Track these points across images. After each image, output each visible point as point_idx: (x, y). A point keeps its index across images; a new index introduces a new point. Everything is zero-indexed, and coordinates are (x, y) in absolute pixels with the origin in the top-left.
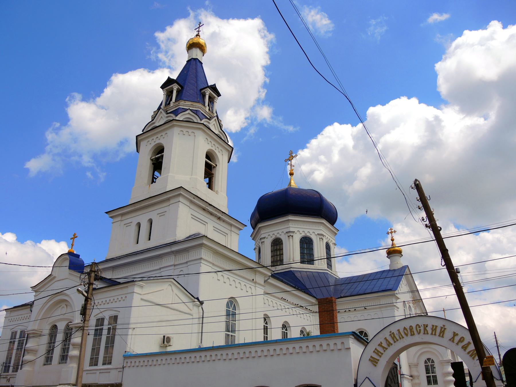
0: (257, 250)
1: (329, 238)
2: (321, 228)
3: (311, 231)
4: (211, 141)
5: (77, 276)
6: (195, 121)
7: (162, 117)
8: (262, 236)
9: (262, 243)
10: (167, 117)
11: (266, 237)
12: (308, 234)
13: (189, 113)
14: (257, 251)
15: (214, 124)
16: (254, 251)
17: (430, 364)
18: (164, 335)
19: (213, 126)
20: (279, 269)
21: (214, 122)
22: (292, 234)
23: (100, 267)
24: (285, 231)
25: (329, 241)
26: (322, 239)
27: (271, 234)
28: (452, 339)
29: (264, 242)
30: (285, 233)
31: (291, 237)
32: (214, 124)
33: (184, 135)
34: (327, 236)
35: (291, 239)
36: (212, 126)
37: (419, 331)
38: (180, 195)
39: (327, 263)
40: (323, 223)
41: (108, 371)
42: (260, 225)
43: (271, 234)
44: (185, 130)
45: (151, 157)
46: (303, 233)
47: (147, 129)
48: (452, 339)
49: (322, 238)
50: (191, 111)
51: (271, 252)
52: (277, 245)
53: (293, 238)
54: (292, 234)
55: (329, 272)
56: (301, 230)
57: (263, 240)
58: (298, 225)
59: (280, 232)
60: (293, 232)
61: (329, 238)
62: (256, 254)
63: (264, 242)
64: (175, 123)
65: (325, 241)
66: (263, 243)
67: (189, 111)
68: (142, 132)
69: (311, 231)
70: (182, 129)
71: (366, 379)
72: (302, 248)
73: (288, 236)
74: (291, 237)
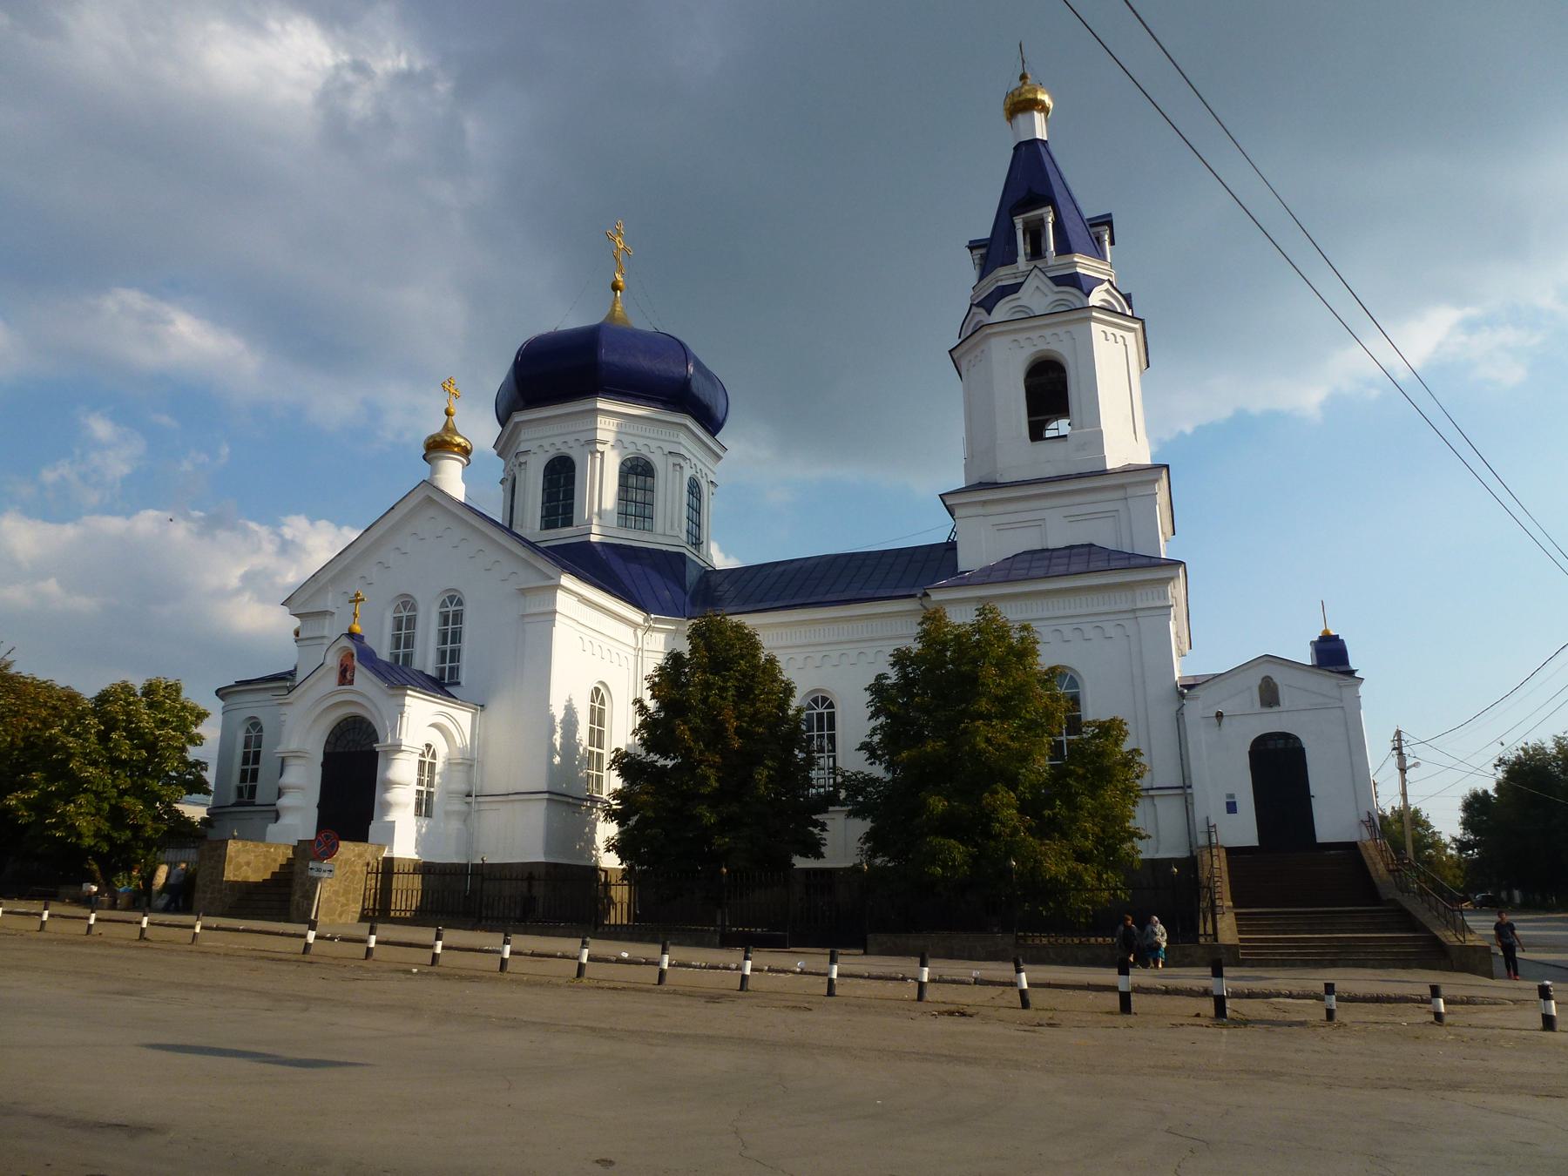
0: (508, 484)
1: (699, 465)
2: (683, 438)
3: (570, 439)
5: (507, 549)
7: (1037, 287)
8: (523, 448)
9: (520, 465)
10: (1057, 293)
12: (645, 451)
14: (508, 486)
15: (1037, 287)
16: (501, 486)
17: (428, 759)
20: (563, 535)
22: (683, 463)
23: (952, 538)
24: (668, 448)
25: (699, 475)
26: (681, 467)
27: (546, 443)
28: (173, 905)
29: (525, 463)
30: (666, 452)
34: (694, 461)
39: (688, 531)
40: (686, 426)
41: (1039, 523)
42: (518, 417)
43: (546, 443)
44: (1019, 336)
47: (965, 334)
48: (173, 905)
49: (679, 465)
55: (689, 552)
57: (522, 459)
58: (640, 429)
59: (570, 439)
60: (685, 458)
61: (699, 465)
62: (505, 496)
63: (525, 463)
64: (989, 331)
65: (688, 473)
66: (523, 467)
68: (960, 340)
69: (653, 445)
72: (623, 485)
73: (674, 465)
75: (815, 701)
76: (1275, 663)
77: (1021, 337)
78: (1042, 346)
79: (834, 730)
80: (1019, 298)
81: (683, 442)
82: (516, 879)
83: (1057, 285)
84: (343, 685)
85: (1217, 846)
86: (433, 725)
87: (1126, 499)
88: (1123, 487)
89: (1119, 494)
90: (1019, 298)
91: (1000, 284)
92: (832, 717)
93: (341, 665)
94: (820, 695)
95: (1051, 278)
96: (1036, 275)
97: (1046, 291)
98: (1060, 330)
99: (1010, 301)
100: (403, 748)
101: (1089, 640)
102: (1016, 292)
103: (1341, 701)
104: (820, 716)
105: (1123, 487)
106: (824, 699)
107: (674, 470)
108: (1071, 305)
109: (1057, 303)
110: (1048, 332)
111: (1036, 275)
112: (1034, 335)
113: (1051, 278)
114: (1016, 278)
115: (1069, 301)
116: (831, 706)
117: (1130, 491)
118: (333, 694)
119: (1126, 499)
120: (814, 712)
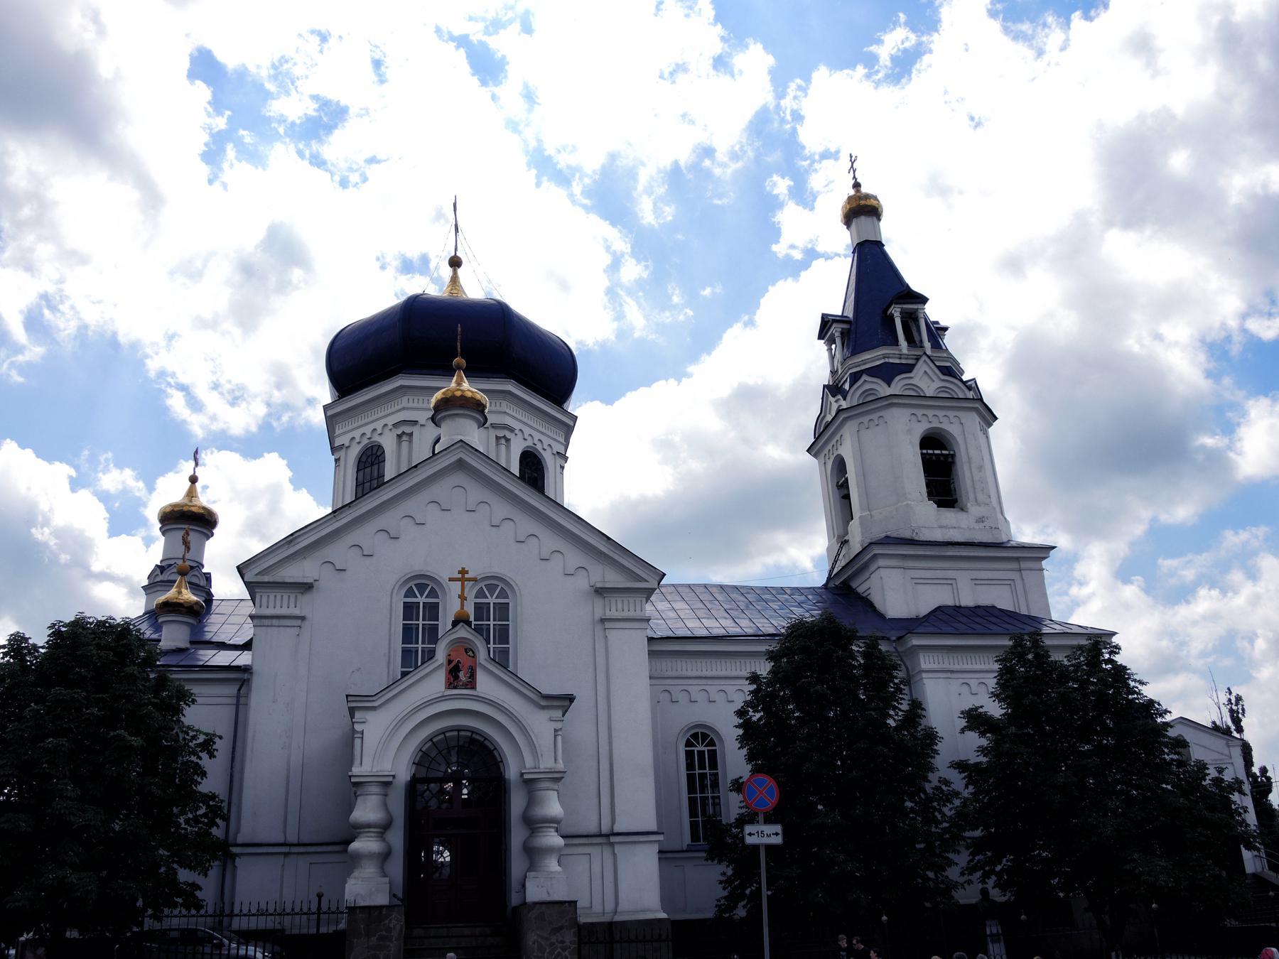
4: (926, 413)
6: (961, 396)
11: (347, 444)
12: (539, 447)
13: (865, 381)
15: (925, 372)
18: (221, 746)
19: (926, 378)
21: (925, 368)
22: (509, 435)
26: (508, 440)
31: (405, 438)
32: (925, 372)
33: (919, 421)
35: (405, 445)
36: (920, 379)
37: (292, 573)
38: (875, 556)
40: (510, 393)
43: (357, 434)
45: (838, 483)
46: (529, 438)
49: (504, 437)
50: (949, 372)
51: (357, 486)
52: (372, 465)
53: (410, 442)
54: (509, 435)
56: (527, 431)
60: (512, 430)
67: (865, 377)
69: (546, 441)
70: (914, 411)
71: (596, 847)
74: (503, 441)
75: (695, 736)
76: (1190, 726)
77: (919, 412)
78: (935, 424)
79: (686, 751)
80: (911, 378)
81: (508, 411)
82: (293, 913)
83: (944, 374)
84: (455, 688)
85: (184, 556)
86: (737, 691)
87: (1020, 570)
88: (1017, 559)
89: (1014, 565)
90: (911, 378)
91: (887, 360)
92: (713, 754)
93: (450, 662)
94: (712, 736)
95: (938, 367)
96: (925, 361)
97: (934, 378)
98: (951, 414)
99: (902, 379)
100: (748, 682)
101: (733, 701)
102: (910, 371)
103: (1231, 758)
104: (701, 753)
105: (1017, 559)
106: (705, 736)
107: (498, 444)
108: (953, 394)
109: (942, 389)
110: (940, 413)
111: (925, 361)
112: (930, 413)
113: (938, 367)
114: (900, 358)
115: (952, 390)
116: (712, 743)
117: (1024, 565)
118: (442, 699)
119: (1020, 570)
120: (696, 749)
